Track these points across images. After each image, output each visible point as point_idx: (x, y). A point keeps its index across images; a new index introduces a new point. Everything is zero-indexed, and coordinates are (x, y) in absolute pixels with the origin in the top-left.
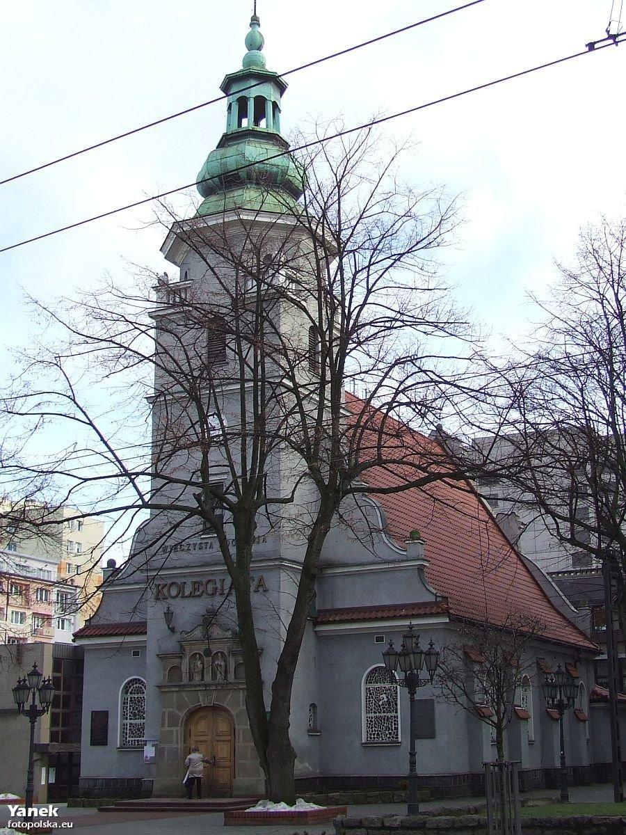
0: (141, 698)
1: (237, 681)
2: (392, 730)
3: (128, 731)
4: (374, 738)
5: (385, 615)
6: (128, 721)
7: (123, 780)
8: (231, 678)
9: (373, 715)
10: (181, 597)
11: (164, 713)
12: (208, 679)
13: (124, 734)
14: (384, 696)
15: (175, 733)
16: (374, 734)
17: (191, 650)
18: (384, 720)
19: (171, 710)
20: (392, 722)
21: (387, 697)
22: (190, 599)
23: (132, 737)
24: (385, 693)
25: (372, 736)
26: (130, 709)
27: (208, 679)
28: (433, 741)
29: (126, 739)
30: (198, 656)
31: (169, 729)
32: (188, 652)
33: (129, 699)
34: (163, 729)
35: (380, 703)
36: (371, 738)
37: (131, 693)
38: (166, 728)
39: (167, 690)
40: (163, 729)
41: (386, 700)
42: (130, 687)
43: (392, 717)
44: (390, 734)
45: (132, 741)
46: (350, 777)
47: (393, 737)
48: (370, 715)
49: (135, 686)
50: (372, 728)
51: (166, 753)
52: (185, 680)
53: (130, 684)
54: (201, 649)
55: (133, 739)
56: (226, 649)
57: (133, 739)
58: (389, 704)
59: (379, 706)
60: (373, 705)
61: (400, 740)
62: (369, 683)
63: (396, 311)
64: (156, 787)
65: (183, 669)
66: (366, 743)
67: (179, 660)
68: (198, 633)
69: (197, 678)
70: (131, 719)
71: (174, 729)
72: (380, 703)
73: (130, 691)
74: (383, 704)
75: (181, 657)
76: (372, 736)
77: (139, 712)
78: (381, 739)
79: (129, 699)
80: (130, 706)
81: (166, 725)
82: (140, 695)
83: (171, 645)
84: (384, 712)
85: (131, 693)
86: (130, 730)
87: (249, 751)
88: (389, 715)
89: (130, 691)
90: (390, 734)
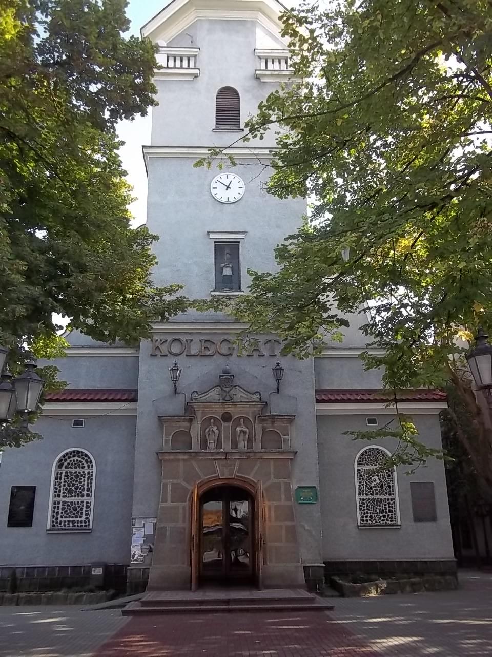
0: (79, 473)
1: (263, 450)
2: (386, 512)
3: (60, 511)
4: (367, 521)
5: (371, 397)
6: (62, 499)
7: (53, 568)
8: (257, 446)
9: (365, 497)
10: (187, 355)
11: (165, 485)
12: (227, 446)
13: (55, 514)
14: (376, 478)
15: (181, 511)
16: (367, 517)
17: (204, 413)
18: (377, 503)
19: (175, 481)
20: (385, 505)
21: (379, 479)
22: (198, 358)
23: (66, 517)
24: (377, 476)
25: (365, 519)
26: (64, 485)
27: (227, 446)
28: (434, 524)
29: (57, 519)
30: (212, 420)
31: (276, 481)
32: (199, 415)
33: (64, 474)
34: (164, 504)
35: (372, 485)
36: (363, 521)
37: (66, 467)
38: (169, 503)
39: (172, 457)
40: (164, 504)
41: (378, 481)
42: (66, 460)
43: (385, 499)
44: (384, 516)
45: (65, 522)
46: (346, 562)
47: (387, 520)
48: (362, 497)
49: (72, 459)
50: (364, 510)
51: (168, 533)
52: (196, 447)
53: (66, 457)
54: (219, 412)
55: (67, 520)
56: (250, 414)
57: (67, 520)
58: (382, 487)
59: (371, 488)
60: (366, 488)
61: (91, 527)
62: (359, 464)
63: (229, 185)
64: (153, 576)
65: (193, 434)
66: (361, 526)
67: (186, 424)
68: (214, 394)
69: (212, 446)
70: (64, 497)
71: (181, 505)
72: (372, 485)
73: (66, 464)
74: (375, 487)
75: (191, 421)
76: (365, 519)
77: (76, 488)
78: (374, 522)
79: (64, 474)
80: (65, 482)
81: (169, 499)
82: (78, 470)
83: (175, 407)
84: (377, 494)
85: (66, 467)
86: (63, 509)
87: (284, 532)
88: (383, 497)
89: (66, 464)
90: (384, 516)
